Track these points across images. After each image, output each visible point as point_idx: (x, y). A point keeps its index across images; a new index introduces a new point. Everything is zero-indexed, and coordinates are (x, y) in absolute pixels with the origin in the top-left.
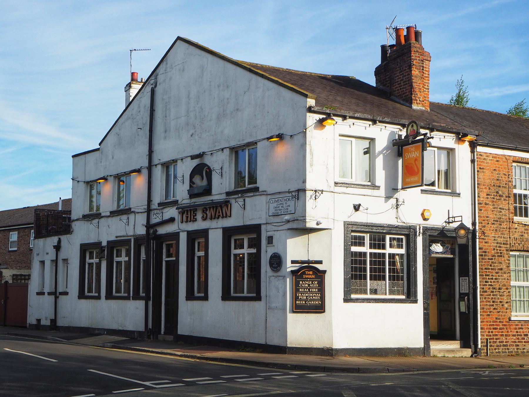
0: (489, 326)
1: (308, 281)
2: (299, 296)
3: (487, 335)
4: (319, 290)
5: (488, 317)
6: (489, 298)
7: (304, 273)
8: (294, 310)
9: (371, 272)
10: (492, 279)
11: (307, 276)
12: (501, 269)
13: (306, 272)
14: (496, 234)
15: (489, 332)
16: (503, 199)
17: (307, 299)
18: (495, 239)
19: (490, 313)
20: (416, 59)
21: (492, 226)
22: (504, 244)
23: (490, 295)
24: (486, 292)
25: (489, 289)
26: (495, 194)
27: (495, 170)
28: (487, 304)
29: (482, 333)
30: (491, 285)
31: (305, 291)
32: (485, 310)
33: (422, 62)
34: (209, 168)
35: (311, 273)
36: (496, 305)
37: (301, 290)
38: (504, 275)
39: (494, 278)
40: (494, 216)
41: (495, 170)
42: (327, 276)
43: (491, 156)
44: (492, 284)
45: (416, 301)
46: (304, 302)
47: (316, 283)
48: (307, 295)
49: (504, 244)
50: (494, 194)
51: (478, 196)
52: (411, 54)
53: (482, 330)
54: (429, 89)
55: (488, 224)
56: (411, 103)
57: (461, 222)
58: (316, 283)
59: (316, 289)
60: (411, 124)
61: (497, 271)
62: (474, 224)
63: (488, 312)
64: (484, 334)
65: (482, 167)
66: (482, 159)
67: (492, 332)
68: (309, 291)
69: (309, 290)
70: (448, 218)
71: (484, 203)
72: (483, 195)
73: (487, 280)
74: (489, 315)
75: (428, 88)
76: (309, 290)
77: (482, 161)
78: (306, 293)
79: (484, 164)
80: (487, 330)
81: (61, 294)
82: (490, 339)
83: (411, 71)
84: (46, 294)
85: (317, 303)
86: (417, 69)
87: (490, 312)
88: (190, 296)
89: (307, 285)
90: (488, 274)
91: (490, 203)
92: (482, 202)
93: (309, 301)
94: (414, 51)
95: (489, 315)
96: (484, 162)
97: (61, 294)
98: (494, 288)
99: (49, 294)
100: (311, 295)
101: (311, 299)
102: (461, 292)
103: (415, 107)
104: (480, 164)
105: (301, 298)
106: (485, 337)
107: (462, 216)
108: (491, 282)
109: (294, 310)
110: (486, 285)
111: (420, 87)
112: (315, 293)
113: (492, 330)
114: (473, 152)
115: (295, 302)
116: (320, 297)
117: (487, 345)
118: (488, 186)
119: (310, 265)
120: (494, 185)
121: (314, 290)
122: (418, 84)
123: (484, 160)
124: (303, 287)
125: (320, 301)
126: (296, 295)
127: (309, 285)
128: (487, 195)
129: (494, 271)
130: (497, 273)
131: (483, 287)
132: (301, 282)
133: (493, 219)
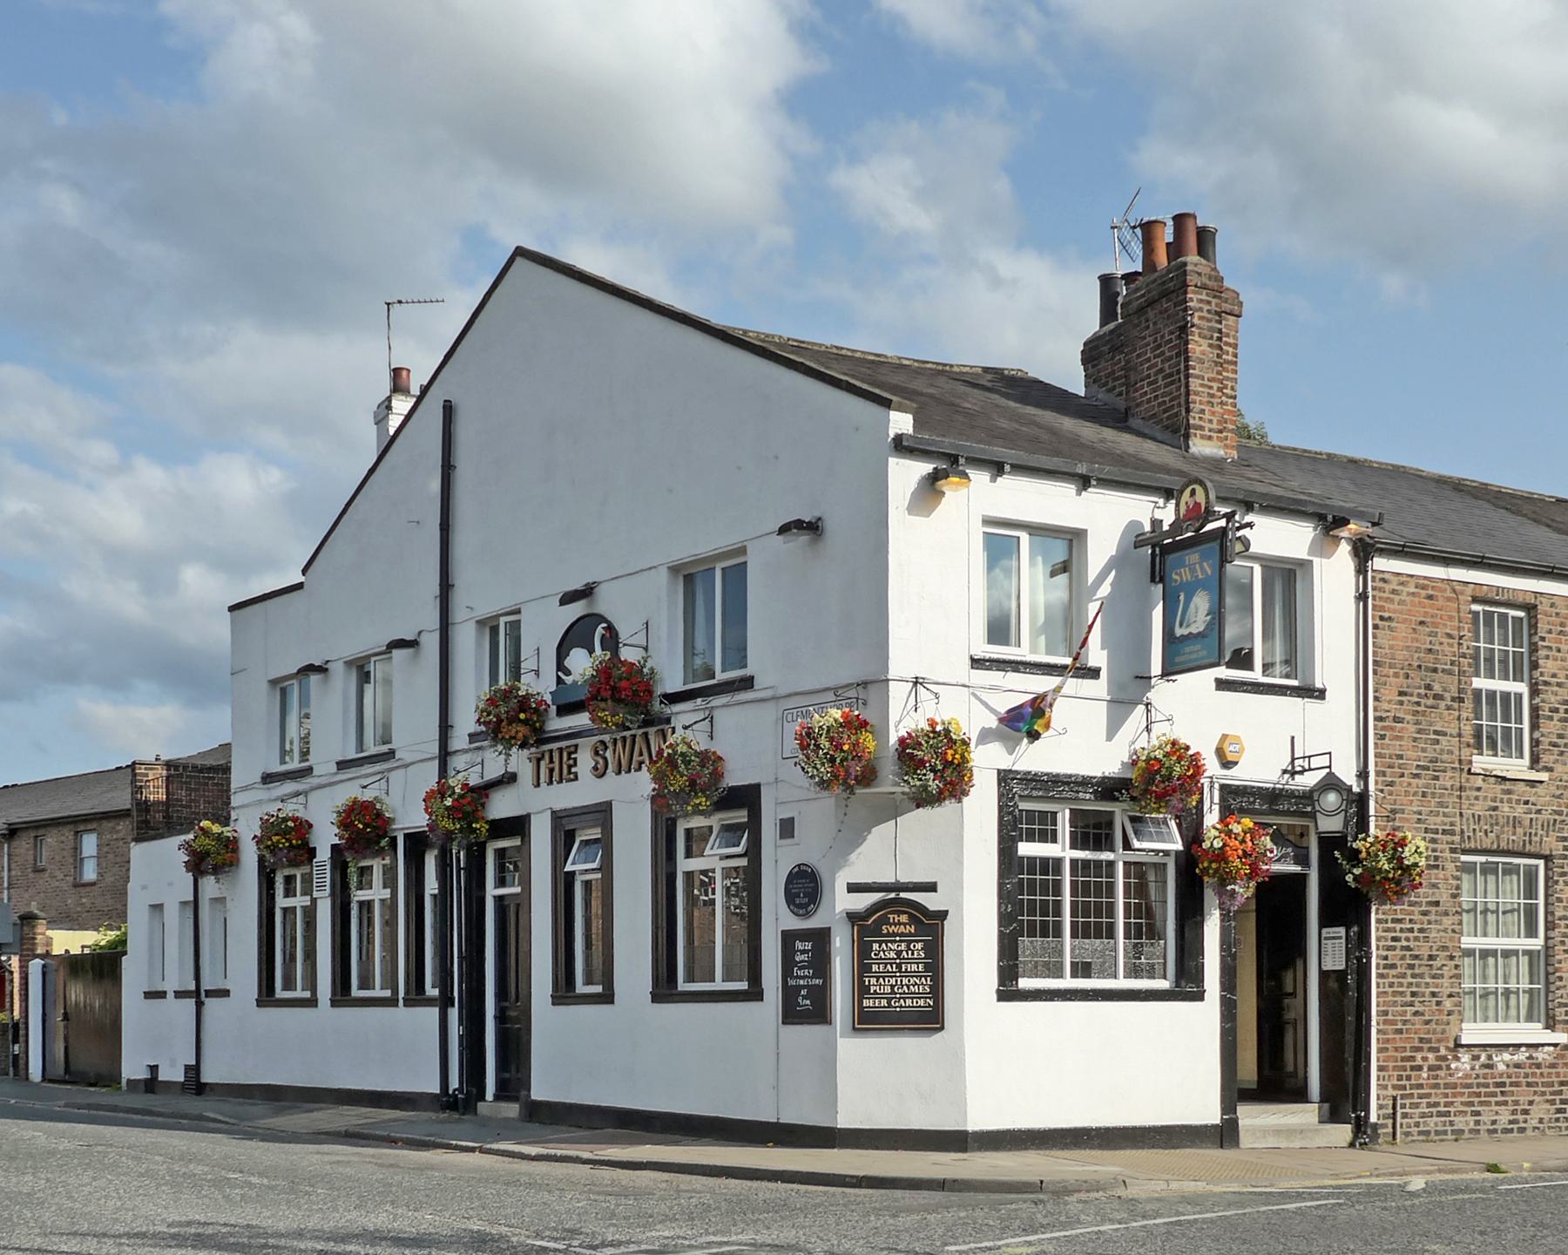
0: (1402, 1061)
1: (895, 941)
2: (869, 985)
3: (1395, 1087)
4: (927, 967)
5: (1398, 1036)
6: (1401, 985)
7: (884, 920)
8: (857, 1026)
9: (1074, 914)
10: (1411, 930)
11: (892, 929)
12: (1437, 904)
13: (891, 916)
14: (1422, 806)
15: (1400, 1078)
16: (1442, 704)
17: (893, 992)
18: (1419, 819)
19: (1404, 1025)
20: (1201, 310)
21: (1414, 781)
22: (1444, 832)
23: (1404, 976)
24: (1393, 966)
25: (1403, 958)
26: (1423, 691)
27: (1422, 623)
28: (1396, 1002)
29: (1381, 1082)
30: (1408, 948)
31: (888, 972)
32: (1390, 1017)
33: (1217, 318)
34: (610, 628)
35: (904, 918)
36: (1420, 1002)
37: (875, 968)
38: (1445, 919)
39: (1416, 927)
40: (1419, 753)
41: (1422, 623)
42: (948, 924)
43: (1413, 582)
44: (1412, 944)
45: (1199, 996)
46: (884, 1002)
47: (919, 946)
48: (893, 981)
49: (1444, 832)
50: (1420, 691)
51: (1376, 699)
52: (1186, 292)
53: (1382, 1074)
54: (1235, 397)
55: (1402, 775)
56: (1187, 436)
57: (1328, 770)
58: (919, 946)
59: (918, 963)
60: (1190, 488)
61: (1423, 908)
62: (1363, 775)
63: (1399, 1023)
64: (1386, 1083)
65: (1386, 615)
66: (1387, 590)
67: (1409, 1078)
68: (900, 972)
69: (899, 966)
70: (1290, 760)
71: (1391, 719)
72: (1390, 694)
73: (1398, 934)
74: (1400, 1031)
75: (1234, 394)
76: (899, 966)
77: (1388, 598)
78: (892, 977)
79: (1391, 606)
80: (1396, 1073)
81: (209, 993)
82: (1403, 1097)
83: (1187, 343)
84: (170, 995)
85: (921, 1002)
86: (1205, 337)
87: (1405, 1022)
88: (564, 992)
89: (893, 955)
90: (1400, 917)
91: (1409, 717)
92: (1384, 715)
93: (900, 998)
94: (1196, 286)
95: (1400, 1031)
96: (1392, 601)
97: (209, 993)
98: (1416, 957)
99: (179, 994)
100: (905, 981)
101: (904, 993)
102: (1325, 968)
103: (1200, 447)
104: (1381, 606)
105: (875, 991)
106: (1391, 1092)
107: (1330, 753)
108: (1407, 939)
109: (857, 1026)
110: (1394, 948)
111: (1211, 392)
112: (916, 977)
113: (1408, 1073)
114: (1361, 570)
115: (860, 1003)
116: (930, 987)
117: (1394, 1114)
118: (1402, 669)
119: (902, 895)
120: (1420, 667)
121: (914, 967)
122: (1206, 382)
123: (1392, 596)
124: (881, 959)
125: (930, 998)
126: (861, 982)
127: (899, 953)
128: (1401, 694)
129: (1416, 909)
130: (1425, 914)
131: (1385, 953)
132: (875, 946)
133: (1415, 763)
